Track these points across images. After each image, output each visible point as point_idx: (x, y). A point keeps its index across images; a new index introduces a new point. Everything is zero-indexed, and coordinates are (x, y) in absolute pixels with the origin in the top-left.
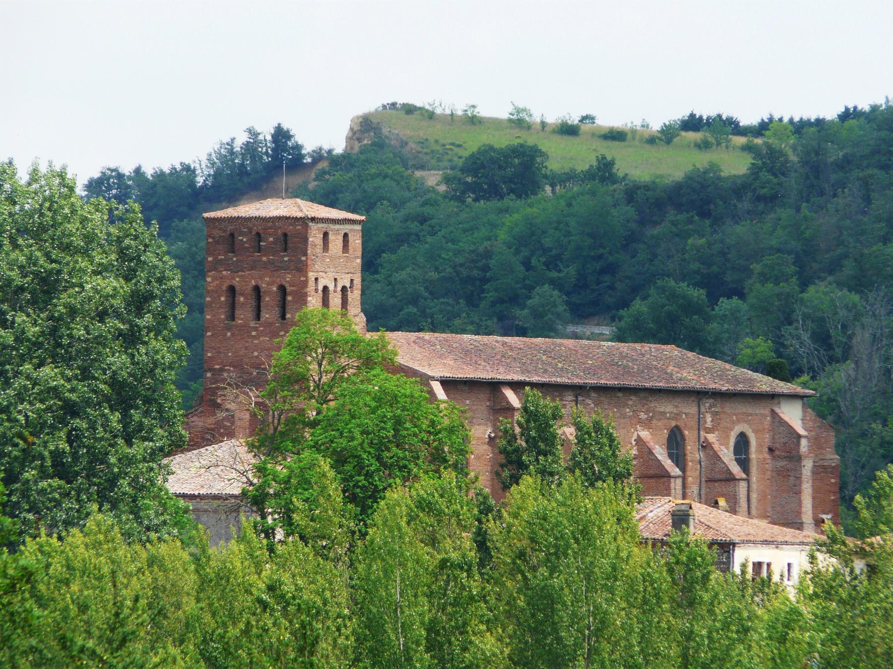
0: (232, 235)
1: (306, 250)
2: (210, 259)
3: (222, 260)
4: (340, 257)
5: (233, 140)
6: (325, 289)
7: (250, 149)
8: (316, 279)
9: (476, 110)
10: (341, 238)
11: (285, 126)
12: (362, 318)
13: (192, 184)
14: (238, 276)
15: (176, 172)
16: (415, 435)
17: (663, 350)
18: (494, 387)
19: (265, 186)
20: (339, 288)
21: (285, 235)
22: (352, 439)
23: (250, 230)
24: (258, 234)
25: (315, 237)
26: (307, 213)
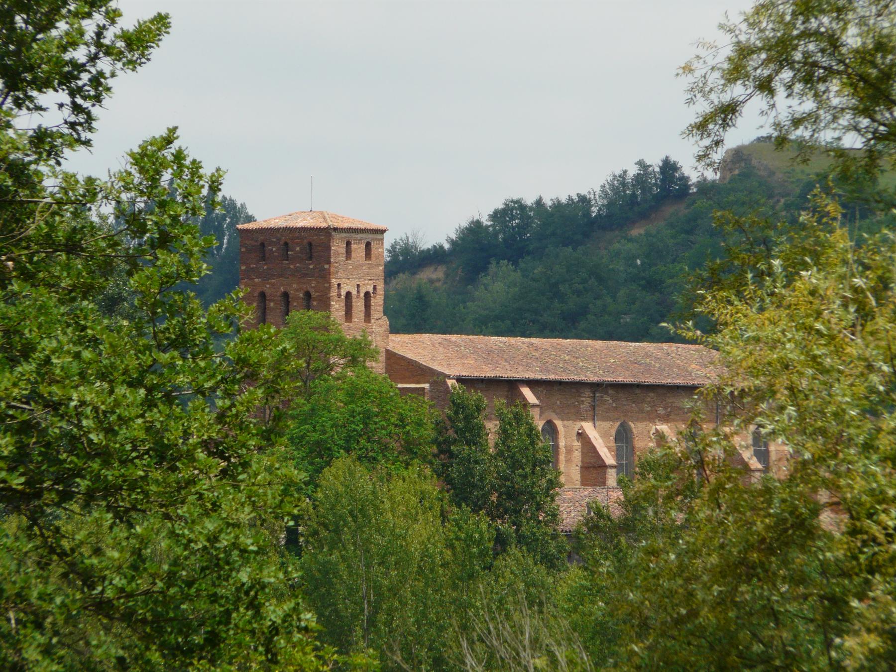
0: (263, 245)
1: (329, 257)
2: (243, 268)
3: (253, 268)
4: (362, 265)
5: (625, 172)
6: (348, 294)
7: (640, 180)
8: (339, 285)
9: (842, 142)
10: (363, 247)
11: (673, 159)
12: (385, 322)
13: (588, 213)
14: (269, 284)
15: (573, 202)
16: (383, 428)
17: (690, 350)
18: (511, 386)
19: (653, 215)
20: (362, 294)
21: (310, 244)
22: (324, 432)
23: (279, 240)
24: (286, 244)
25: (337, 247)
26: (330, 223)
